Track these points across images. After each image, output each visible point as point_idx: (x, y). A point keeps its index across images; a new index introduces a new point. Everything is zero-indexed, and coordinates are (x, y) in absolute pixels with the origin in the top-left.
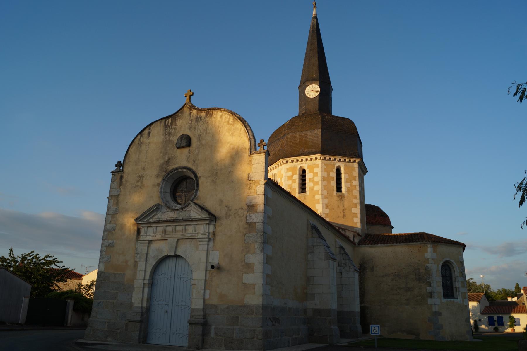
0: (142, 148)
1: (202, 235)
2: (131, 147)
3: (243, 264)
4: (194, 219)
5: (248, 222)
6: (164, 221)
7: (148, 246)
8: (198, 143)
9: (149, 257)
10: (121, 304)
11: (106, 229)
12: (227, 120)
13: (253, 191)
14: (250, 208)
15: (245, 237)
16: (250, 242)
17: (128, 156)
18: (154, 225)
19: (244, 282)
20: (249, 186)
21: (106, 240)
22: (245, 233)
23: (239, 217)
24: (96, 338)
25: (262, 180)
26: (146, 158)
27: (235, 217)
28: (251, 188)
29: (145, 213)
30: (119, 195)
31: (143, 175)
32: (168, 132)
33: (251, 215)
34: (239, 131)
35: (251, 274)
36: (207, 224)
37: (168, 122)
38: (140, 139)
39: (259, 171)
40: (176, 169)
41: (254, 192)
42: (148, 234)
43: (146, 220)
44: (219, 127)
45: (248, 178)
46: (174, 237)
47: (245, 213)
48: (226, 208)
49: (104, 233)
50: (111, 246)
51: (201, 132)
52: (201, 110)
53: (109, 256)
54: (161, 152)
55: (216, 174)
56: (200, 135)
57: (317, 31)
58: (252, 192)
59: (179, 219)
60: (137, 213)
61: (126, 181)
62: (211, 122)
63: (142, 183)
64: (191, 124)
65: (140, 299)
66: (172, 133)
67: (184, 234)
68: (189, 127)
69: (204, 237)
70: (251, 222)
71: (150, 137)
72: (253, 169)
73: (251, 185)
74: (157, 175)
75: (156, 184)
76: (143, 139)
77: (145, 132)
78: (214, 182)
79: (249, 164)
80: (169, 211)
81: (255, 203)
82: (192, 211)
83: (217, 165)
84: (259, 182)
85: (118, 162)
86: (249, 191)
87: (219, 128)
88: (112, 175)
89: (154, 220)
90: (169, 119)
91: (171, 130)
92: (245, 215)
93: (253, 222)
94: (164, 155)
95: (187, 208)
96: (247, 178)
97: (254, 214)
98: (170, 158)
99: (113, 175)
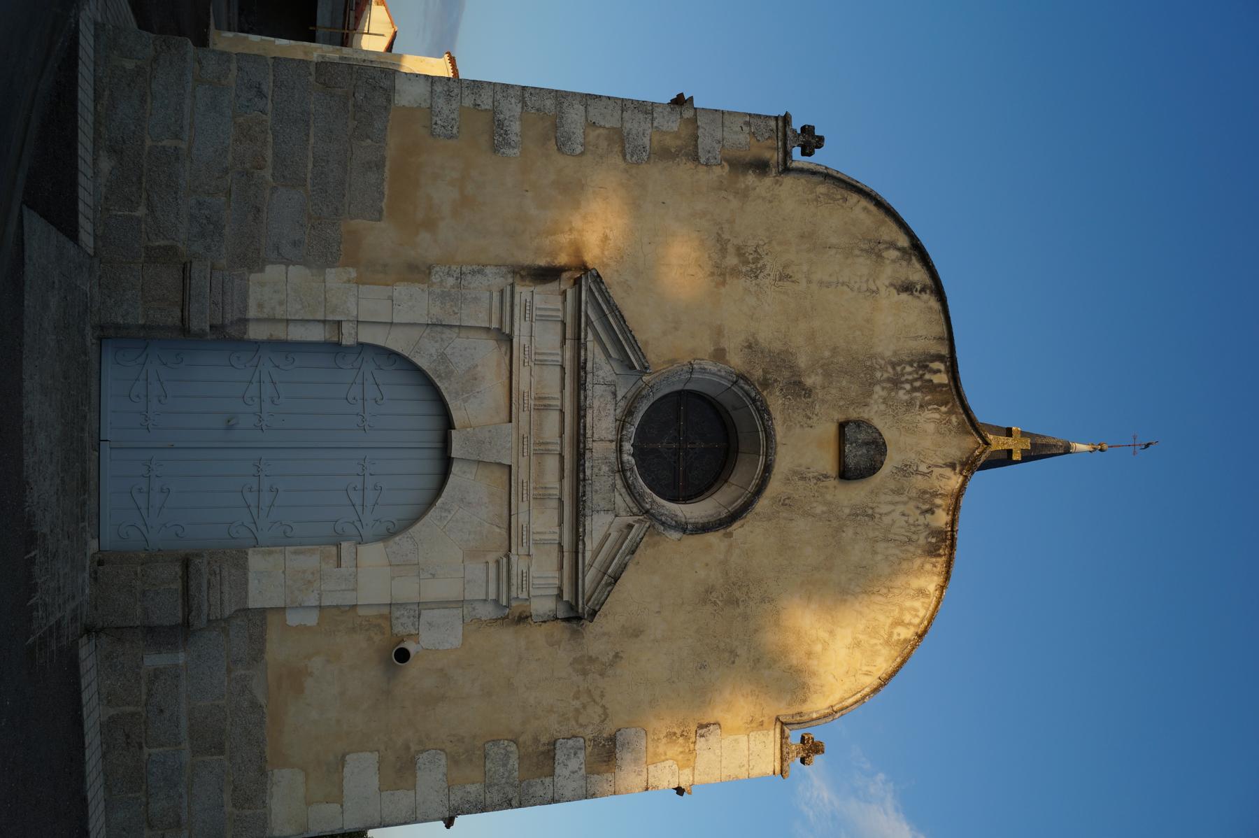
0: (861, 260)
1: (520, 573)
2: (872, 207)
3: (413, 748)
4: (580, 543)
5: (558, 745)
6: (582, 413)
7: (488, 329)
8: (847, 511)
9: (448, 333)
10: (258, 210)
11: (565, 105)
12: (907, 618)
13: (661, 749)
14: (604, 745)
15: (506, 742)
16: (489, 765)
17: (840, 193)
18: (568, 354)
19: (347, 757)
20: (678, 732)
21: (522, 108)
22: (521, 740)
23: (577, 710)
24: (107, 93)
25: (693, 776)
26: (821, 283)
27: (576, 697)
28: (670, 742)
29: (621, 319)
30: (695, 158)
31: (762, 275)
32: (903, 375)
33: (581, 755)
34: (865, 668)
35: (375, 781)
36: (560, 589)
37: (939, 371)
38: (892, 245)
39: (724, 763)
40: (769, 436)
41: (656, 754)
42: (537, 327)
43: (593, 317)
44: (889, 589)
45: (707, 726)
46: (520, 451)
47: (589, 732)
48: (611, 654)
49: (550, 91)
50: (497, 136)
51: (884, 518)
52: (955, 510)
53: (455, 131)
54: (834, 350)
55: (733, 602)
56: (872, 517)
57: (1034, 456)
58: (658, 747)
59: (587, 464)
60: (622, 257)
61: (744, 195)
62: (909, 555)
63: (735, 272)
64: (917, 472)
65: (279, 313)
66: (897, 393)
67: (528, 495)
68: (906, 466)
69: (514, 581)
70: (557, 757)
71: (895, 292)
72: (732, 738)
73: (681, 740)
74: (757, 342)
75: (725, 344)
76: (894, 261)
77: (917, 265)
78: (706, 595)
79: (752, 721)
80: (618, 411)
81: (619, 763)
82: (610, 517)
83: (763, 601)
84: (688, 767)
85: (821, 139)
86: (662, 736)
87: (884, 591)
88: (776, 118)
89: (590, 345)
90: (947, 372)
91: (908, 386)
92: (581, 730)
93: (556, 764)
94: (822, 366)
95: (624, 490)
96: (705, 722)
97: (583, 766)
98: (809, 397)
99: (773, 123)
